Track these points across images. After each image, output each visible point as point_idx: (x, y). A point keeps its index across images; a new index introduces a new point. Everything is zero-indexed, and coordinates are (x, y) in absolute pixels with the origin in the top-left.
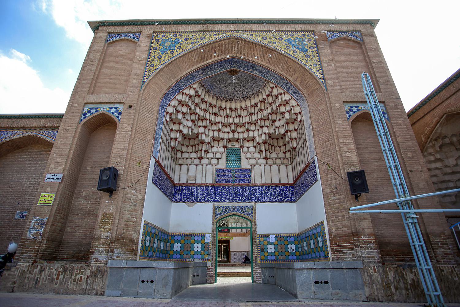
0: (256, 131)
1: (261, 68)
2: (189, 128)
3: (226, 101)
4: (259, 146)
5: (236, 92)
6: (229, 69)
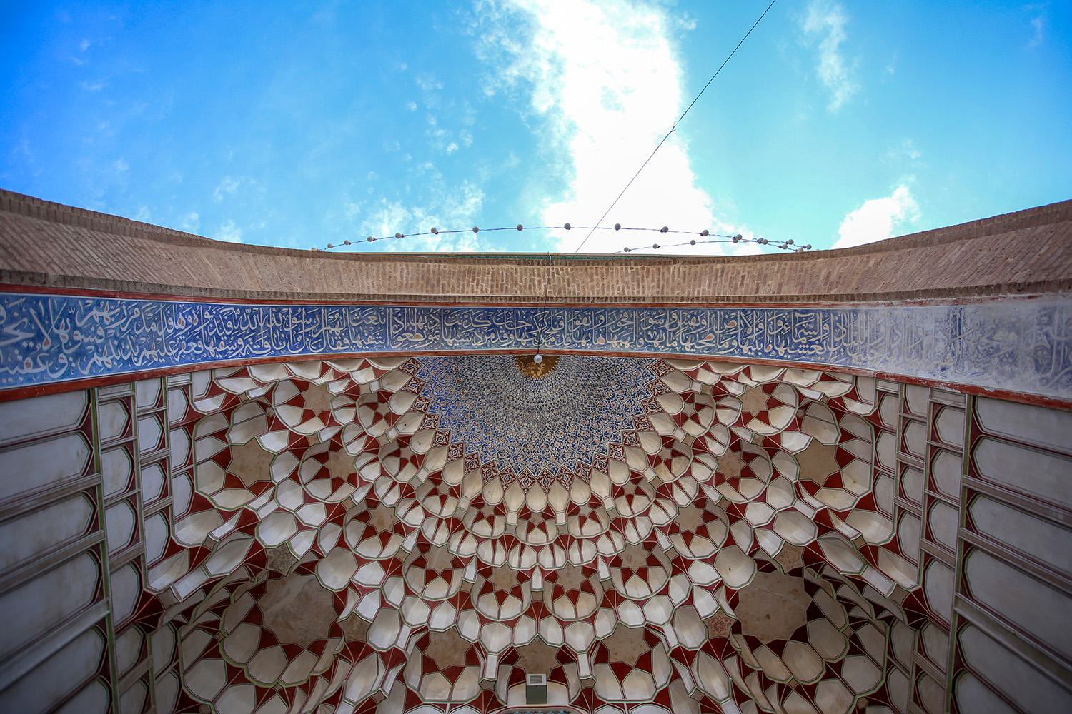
0: (654, 600)
1: (635, 314)
2: (301, 527)
3: (506, 485)
4: (691, 673)
5: (549, 443)
6: (521, 348)
